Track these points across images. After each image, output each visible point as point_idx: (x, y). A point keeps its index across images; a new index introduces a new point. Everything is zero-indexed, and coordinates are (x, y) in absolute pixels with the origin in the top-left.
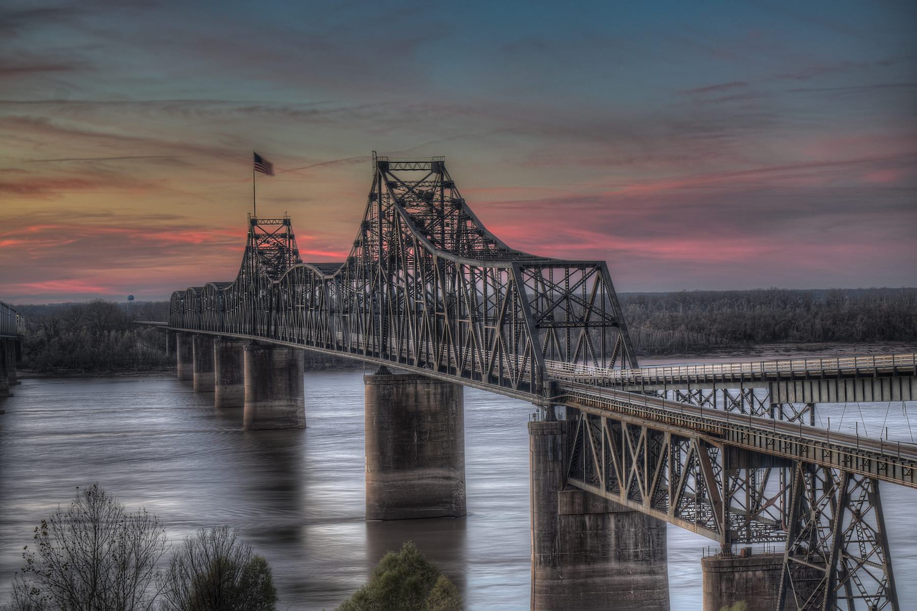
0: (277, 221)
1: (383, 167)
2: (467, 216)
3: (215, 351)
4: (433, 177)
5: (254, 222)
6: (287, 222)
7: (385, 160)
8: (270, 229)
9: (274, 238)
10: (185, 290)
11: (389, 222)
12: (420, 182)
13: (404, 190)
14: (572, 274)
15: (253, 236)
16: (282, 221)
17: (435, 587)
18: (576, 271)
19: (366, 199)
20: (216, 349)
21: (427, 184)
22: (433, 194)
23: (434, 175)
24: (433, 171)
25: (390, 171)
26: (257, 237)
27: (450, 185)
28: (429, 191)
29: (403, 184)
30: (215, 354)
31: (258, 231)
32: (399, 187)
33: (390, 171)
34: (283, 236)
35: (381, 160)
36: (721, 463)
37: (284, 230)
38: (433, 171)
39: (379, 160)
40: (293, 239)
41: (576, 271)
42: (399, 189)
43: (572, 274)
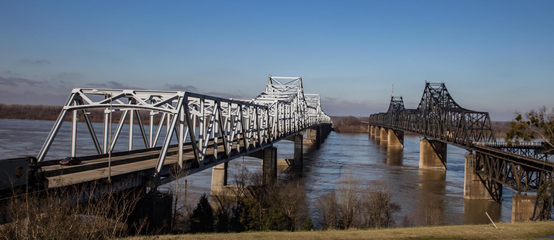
6: (401, 98)
7: (428, 82)
8: (397, 100)
12: (437, 89)
15: (392, 101)
34: (400, 101)
37: (400, 100)
39: (427, 82)
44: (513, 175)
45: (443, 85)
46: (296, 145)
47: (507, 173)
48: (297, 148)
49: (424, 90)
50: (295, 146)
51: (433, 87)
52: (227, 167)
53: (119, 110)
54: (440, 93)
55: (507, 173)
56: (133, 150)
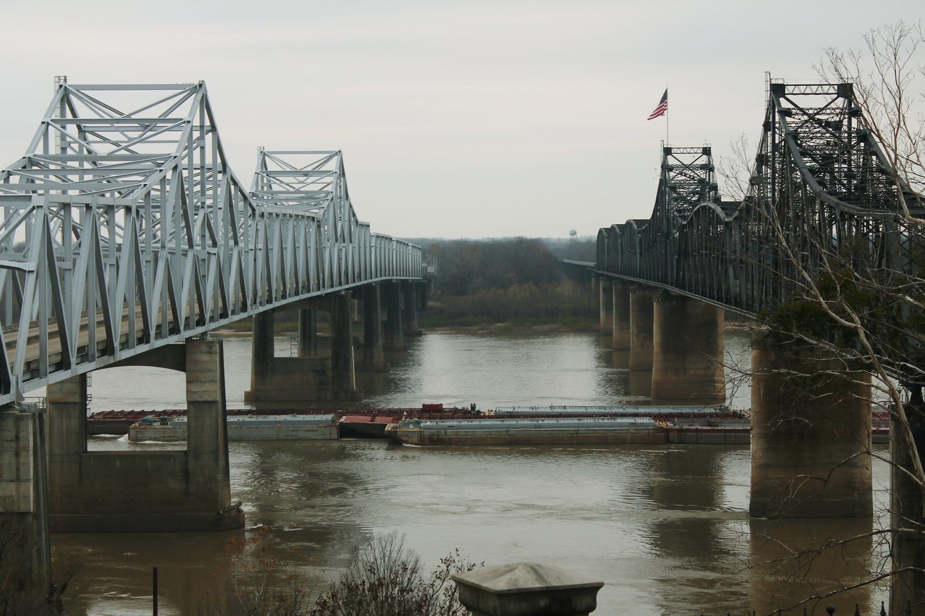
0: (695, 150)
1: (778, 90)
2: (871, 150)
3: (631, 301)
4: (841, 102)
5: (668, 151)
6: (707, 151)
7: (780, 82)
8: (687, 160)
9: (692, 170)
10: (609, 227)
11: (780, 153)
12: (822, 109)
13: (799, 119)
14: (679, 161)
15: (666, 168)
16: (701, 149)
17: (747, 541)
18: (694, 162)
19: (761, 129)
20: (632, 298)
21: (828, 111)
22: (841, 122)
23: (841, 100)
24: (839, 95)
25: (786, 96)
26: (671, 169)
27: (855, 113)
28: (829, 120)
29: (803, 111)
30: (631, 303)
31: (671, 161)
32: (794, 115)
33: (786, 96)
34: (703, 167)
35: (776, 83)
36: (73, 100)
37: (704, 160)
38: (839, 95)
39: (773, 82)
40: (713, 171)
41: (694, 162)
42: (794, 118)
43: (679, 161)
44: (682, 180)
45: (845, 90)
46: (196, 388)
47: (682, 186)
48: (197, 398)
49: (763, 119)
50: (188, 392)
51: (802, 102)
52: (86, 400)
53: (44, 177)
54: (838, 126)
55: (682, 186)
56: (187, 244)
